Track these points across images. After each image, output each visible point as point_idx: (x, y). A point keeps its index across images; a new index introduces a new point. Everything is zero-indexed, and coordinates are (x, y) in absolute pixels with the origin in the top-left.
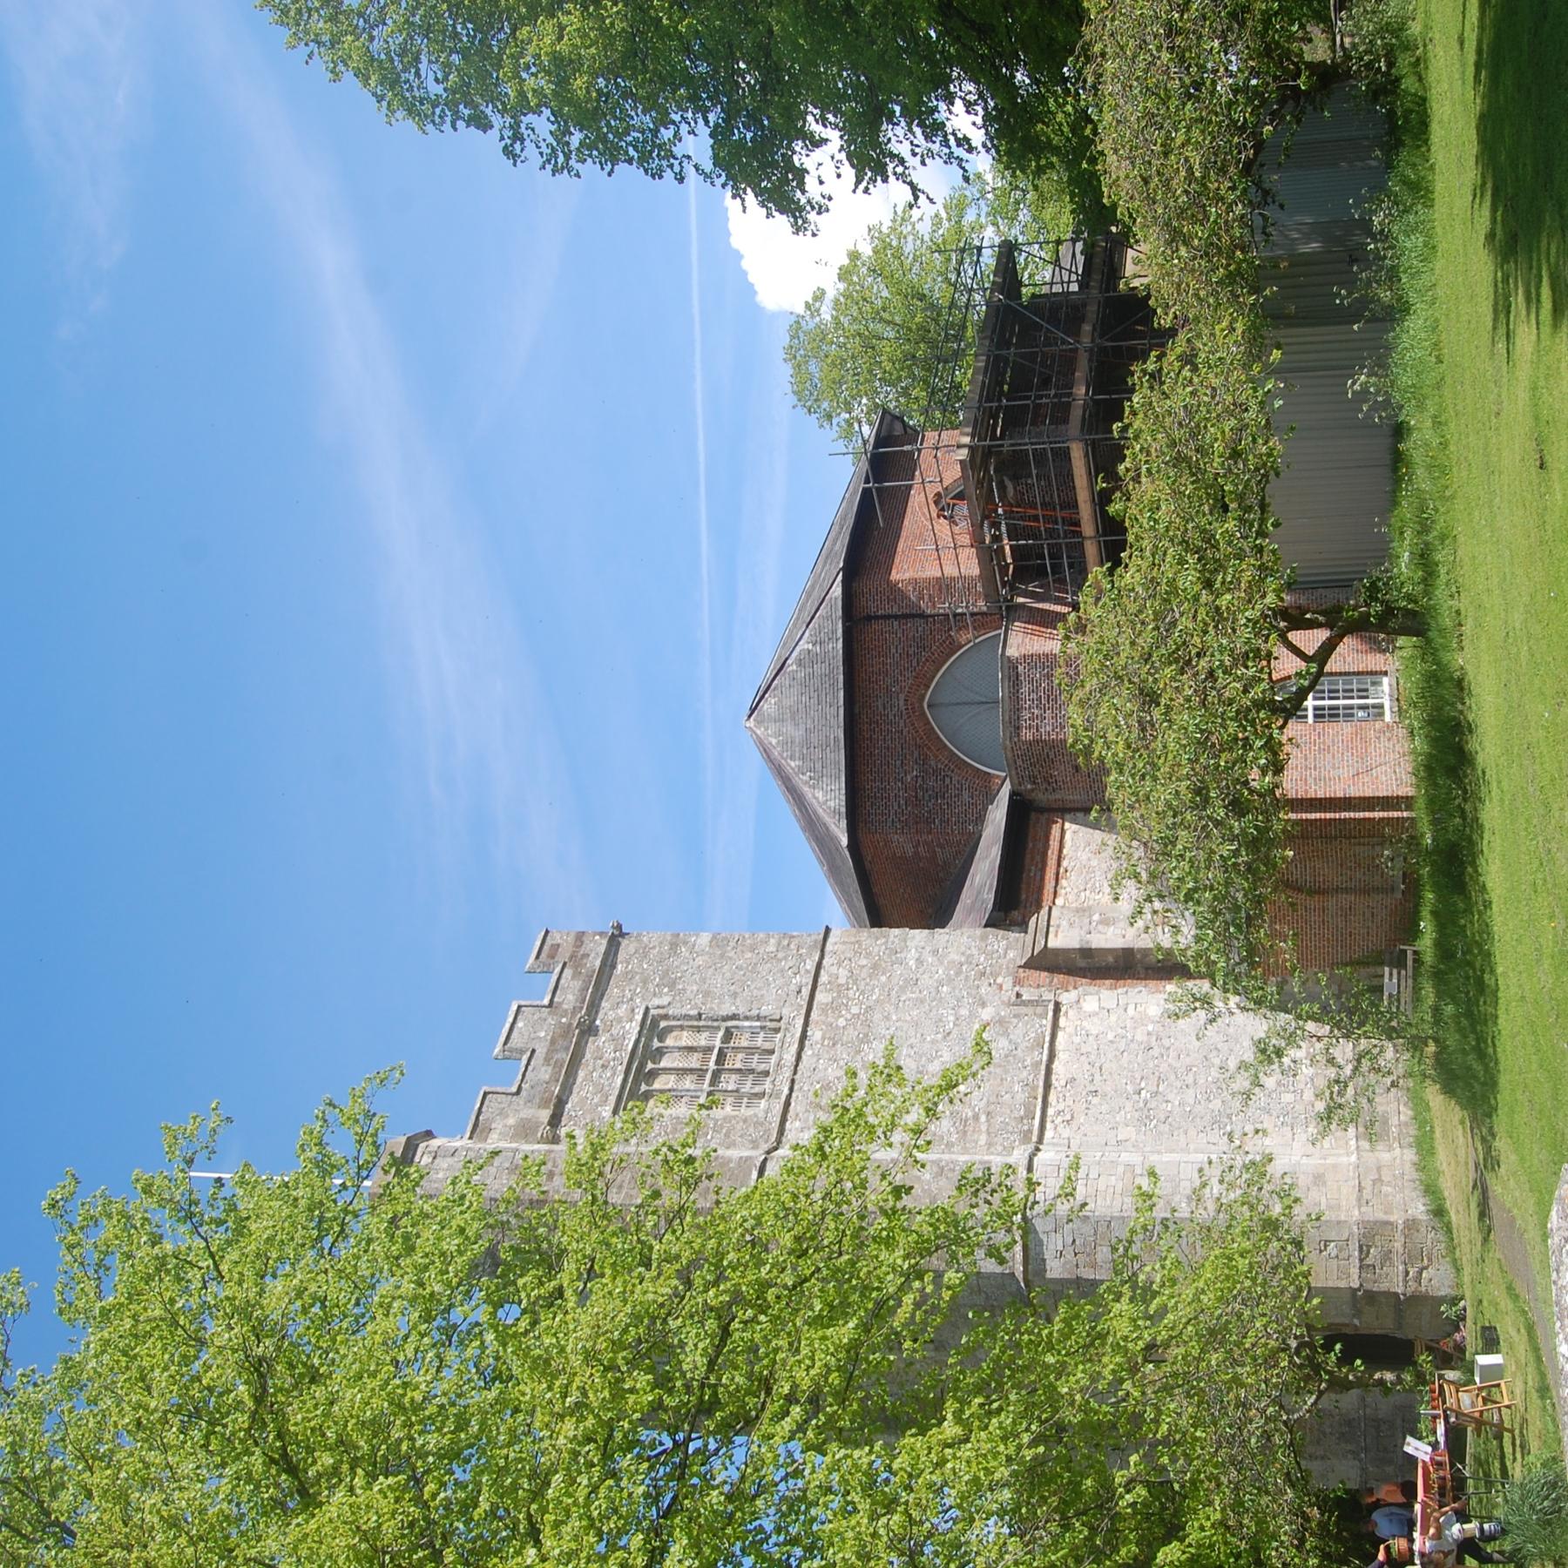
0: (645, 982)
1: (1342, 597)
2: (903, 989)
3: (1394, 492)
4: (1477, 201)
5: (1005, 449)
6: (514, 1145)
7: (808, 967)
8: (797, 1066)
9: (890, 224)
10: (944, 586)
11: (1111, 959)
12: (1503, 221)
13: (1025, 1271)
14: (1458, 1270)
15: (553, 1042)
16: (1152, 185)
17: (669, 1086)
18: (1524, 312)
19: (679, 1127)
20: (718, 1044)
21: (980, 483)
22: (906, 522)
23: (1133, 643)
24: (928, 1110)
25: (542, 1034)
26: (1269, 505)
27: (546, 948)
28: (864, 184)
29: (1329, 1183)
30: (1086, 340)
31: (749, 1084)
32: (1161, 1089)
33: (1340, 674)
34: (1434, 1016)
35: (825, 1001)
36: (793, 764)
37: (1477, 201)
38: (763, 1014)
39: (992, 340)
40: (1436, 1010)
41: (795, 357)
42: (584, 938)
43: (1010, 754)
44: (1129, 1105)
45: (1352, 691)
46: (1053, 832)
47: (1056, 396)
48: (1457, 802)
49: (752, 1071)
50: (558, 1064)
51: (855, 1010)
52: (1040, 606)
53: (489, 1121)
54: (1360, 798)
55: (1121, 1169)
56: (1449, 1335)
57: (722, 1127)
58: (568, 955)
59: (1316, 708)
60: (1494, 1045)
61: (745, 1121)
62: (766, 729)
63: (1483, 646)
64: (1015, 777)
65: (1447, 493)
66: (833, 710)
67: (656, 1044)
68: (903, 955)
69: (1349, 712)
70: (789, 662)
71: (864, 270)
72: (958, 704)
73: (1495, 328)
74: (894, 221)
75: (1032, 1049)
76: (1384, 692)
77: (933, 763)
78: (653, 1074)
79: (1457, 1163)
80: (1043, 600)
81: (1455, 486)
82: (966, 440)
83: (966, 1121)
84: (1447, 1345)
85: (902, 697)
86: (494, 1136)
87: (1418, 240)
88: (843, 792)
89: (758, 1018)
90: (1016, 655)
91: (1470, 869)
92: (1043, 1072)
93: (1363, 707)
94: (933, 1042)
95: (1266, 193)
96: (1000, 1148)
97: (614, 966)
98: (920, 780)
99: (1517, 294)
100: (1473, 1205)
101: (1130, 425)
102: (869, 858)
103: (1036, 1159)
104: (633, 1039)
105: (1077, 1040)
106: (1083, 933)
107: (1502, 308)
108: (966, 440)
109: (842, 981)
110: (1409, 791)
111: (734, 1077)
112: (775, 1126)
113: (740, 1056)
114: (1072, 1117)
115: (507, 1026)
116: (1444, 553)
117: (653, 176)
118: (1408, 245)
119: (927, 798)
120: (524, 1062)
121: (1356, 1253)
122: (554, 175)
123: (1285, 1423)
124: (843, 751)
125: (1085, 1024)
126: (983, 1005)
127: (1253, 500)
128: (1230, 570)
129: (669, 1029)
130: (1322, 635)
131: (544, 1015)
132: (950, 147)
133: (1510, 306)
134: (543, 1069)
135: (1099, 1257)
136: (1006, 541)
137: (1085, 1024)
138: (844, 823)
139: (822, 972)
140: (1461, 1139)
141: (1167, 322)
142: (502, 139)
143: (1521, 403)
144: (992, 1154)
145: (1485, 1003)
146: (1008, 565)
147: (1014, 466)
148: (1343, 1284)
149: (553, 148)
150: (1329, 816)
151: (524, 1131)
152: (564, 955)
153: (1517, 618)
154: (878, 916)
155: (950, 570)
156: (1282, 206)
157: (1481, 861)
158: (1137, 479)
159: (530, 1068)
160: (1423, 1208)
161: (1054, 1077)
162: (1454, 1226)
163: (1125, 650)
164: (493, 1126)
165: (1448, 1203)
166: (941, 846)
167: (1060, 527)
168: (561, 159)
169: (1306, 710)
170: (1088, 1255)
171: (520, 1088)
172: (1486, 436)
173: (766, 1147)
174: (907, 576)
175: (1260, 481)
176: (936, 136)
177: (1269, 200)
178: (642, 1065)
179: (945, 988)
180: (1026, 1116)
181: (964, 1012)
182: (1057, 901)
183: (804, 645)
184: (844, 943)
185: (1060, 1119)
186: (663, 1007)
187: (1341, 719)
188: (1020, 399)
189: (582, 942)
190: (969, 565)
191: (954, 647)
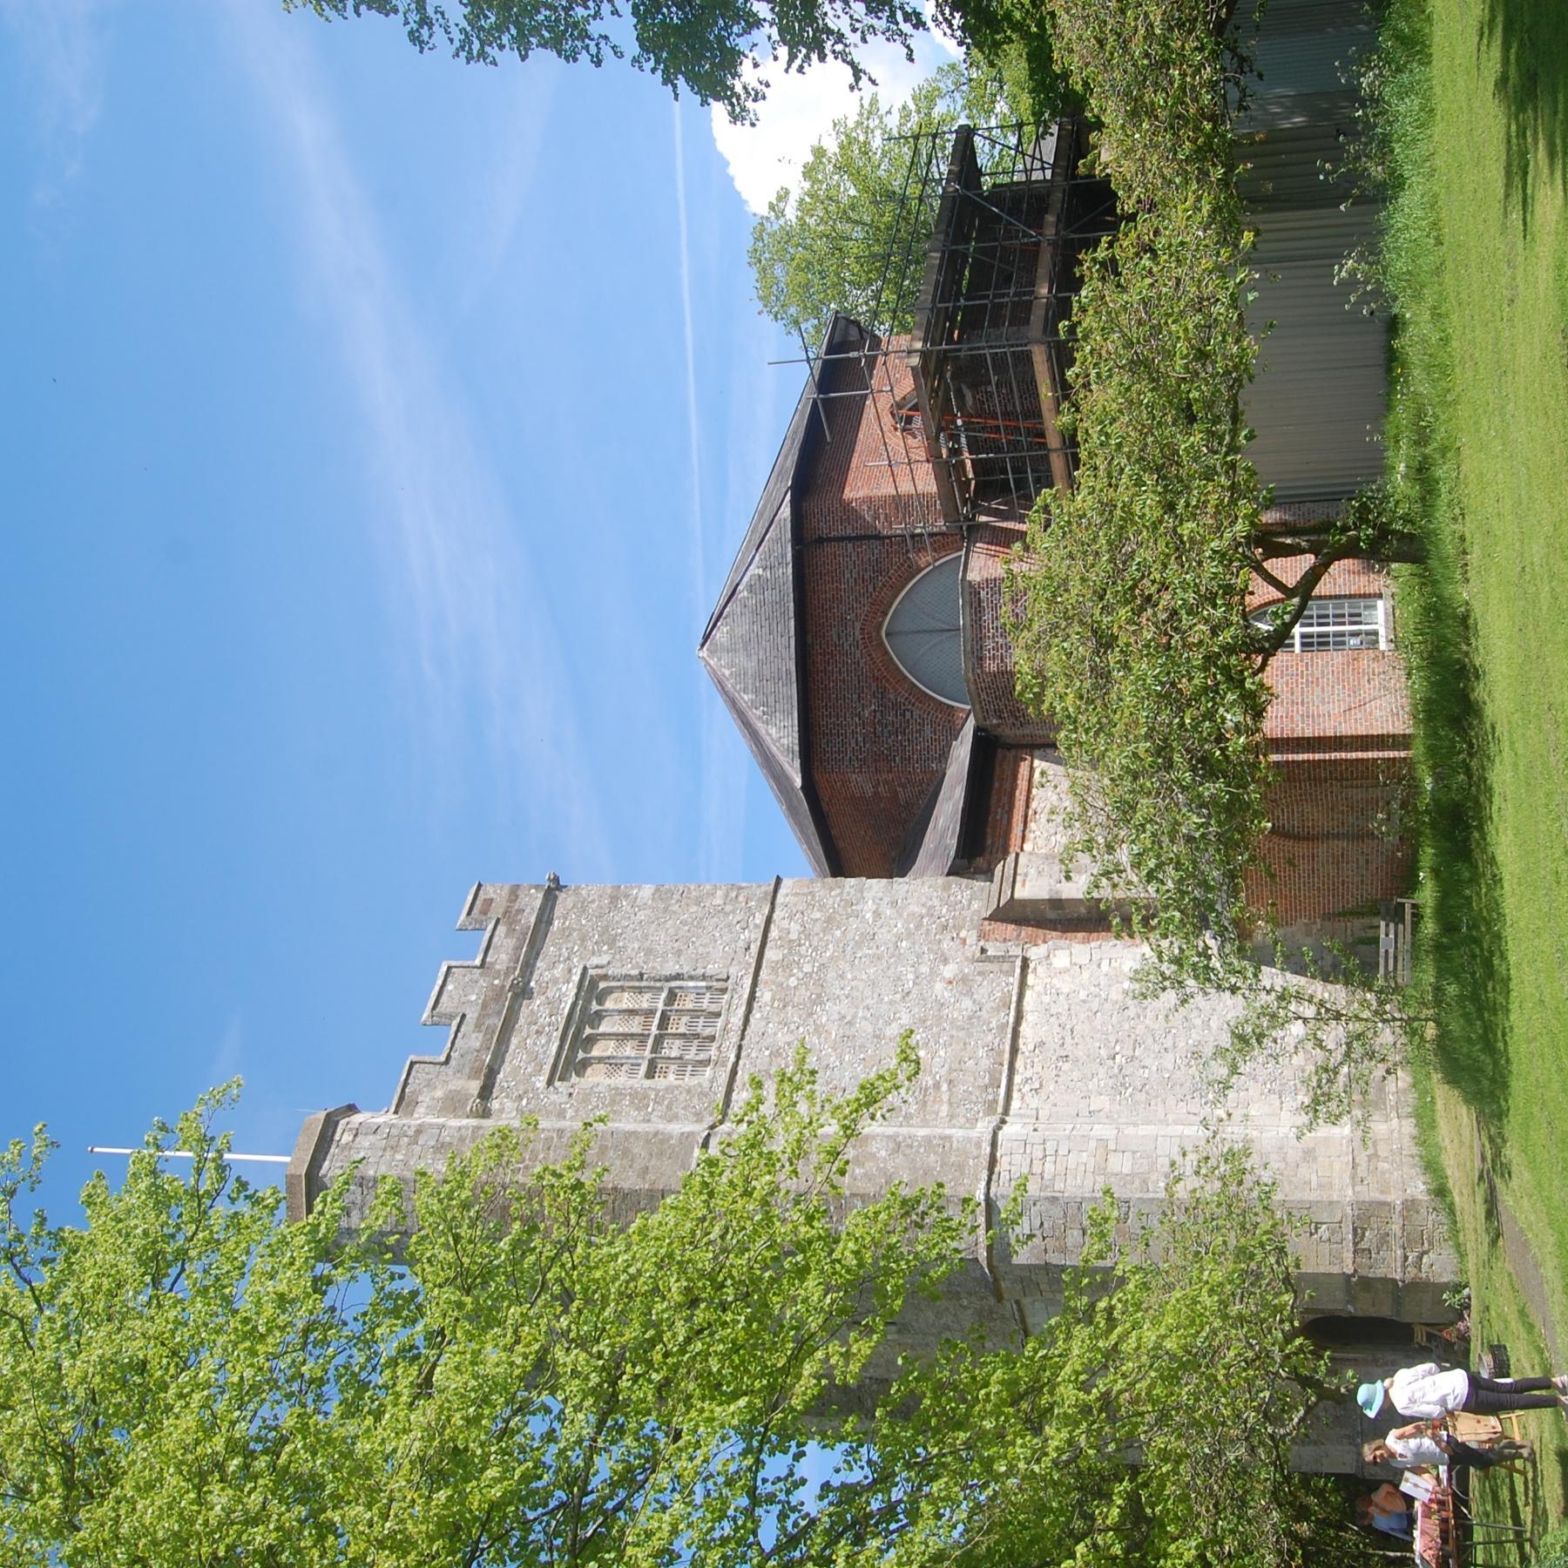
0: (583, 939)
1: (1332, 513)
2: (859, 945)
3: (1388, 395)
4: (1485, 41)
5: (962, 354)
6: (441, 1120)
7: (758, 922)
8: (744, 1031)
9: (857, 118)
10: (900, 504)
11: (1083, 910)
12: (1517, 60)
13: (989, 1258)
14: (1462, 1255)
15: (484, 1006)
16: (1108, 47)
17: (608, 1053)
18: (1546, 171)
19: (618, 1098)
20: (660, 1006)
21: (934, 391)
22: (860, 436)
23: (1083, 580)
24: (846, 1127)
25: (473, 998)
26: (1242, 413)
27: (479, 903)
28: (798, 62)
29: (1320, 1159)
30: (1050, 232)
31: (694, 1050)
32: (1137, 1053)
33: (1330, 597)
34: (1435, 996)
35: (775, 958)
36: (746, 697)
37: (1485, 41)
38: (709, 973)
39: (947, 234)
40: (1438, 990)
41: (760, 261)
42: (519, 892)
43: (973, 687)
44: (1102, 1071)
45: (1344, 616)
46: (1021, 770)
47: (1015, 294)
48: (1461, 756)
49: (697, 1036)
50: (489, 1031)
51: (807, 968)
52: (1004, 525)
53: (416, 1093)
54: (1352, 737)
55: (1093, 1144)
56: (1452, 1324)
57: (664, 1098)
58: (501, 910)
59: (1303, 636)
60: (1506, 1043)
61: (688, 1091)
62: (719, 659)
63: (1493, 580)
64: (979, 711)
65: (1449, 398)
66: (784, 641)
67: (595, 1007)
68: (859, 907)
69: (1339, 641)
70: (741, 588)
71: (830, 167)
72: (919, 632)
73: (1507, 196)
74: (861, 114)
75: (998, 1010)
76: (1379, 618)
77: (892, 696)
78: (591, 1041)
79: (1461, 1142)
80: (1006, 519)
81: (1458, 389)
82: (919, 345)
83: (926, 1090)
84: (1450, 1334)
85: (858, 625)
86: (421, 1110)
87: (1413, 103)
88: (796, 729)
89: (704, 977)
90: (978, 579)
91: (1476, 834)
92: (1009, 1036)
93: (1354, 634)
94: (891, 1003)
95: (1242, 60)
96: (962, 1120)
97: (550, 922)
98: (878, 715)
99: (1536, 149)
100: (1480, 1199)
101: (1079, 323)
102: (827, 799)
103: (1000, 1133)
104: (570, 1002)
105: (1047, 999)
106: (1052, 882)
107: (1517, 169)
108: (919, 345)
109: (794, 936)
110: (1400, 725)
111: (678, 1043)
112: (720, 1097)
113: (685, 1019)
114: (1041, 1085)
115: (437, 988)
116: (1445, 468)
117: (567, 59)
118: (1402, 109)
119: (886, 734)
120: (454, 1028)
121: (1350, 1236)
122: (468, 63)
123: (1272, 1437)
124: (795, 685)
125: (1055, 981)
126: (945, 961)
127: (1222, 408)
128: (1195, 492)
129: (609, 991)
130: (1308, 560)
131: (475, 977)
132: (897, 24)
133: (1527, 165)
134: (474, 1035)
135: (1070, 1242)
136: (966, 454)
137: (1055, 981)
138: (797, 763)
139: (772, 926)
140: (1465, 1119)
141: (1129, 206)
142: (406, 23)
143: (1542, 288)
144: (954, 1127)
145: (1494, 989)
146: (969, 481)
147: (971, 372)
148: (1335, 1270)
149: (466, 33)
150: (1318, 756)
151: (452, 1104)
152: (497, 911)
153: (1537, 551)
154: (838, 864)
155: (906, 488)
156: (1260, 76)
157: (1490, 828)
158: (1086, 386)
159: (460, 1035)
160: (1423, 1187)
161: (1021, 1041)
162: (1458, 1209)
163: (1075, 587)
164: (420, 1099)
165: (1451, 1182)
166: (903, 786)
167: (1023, 439)
168: (476, 46)
169: (1293, 638)
170: (1058, 1239)
171: (448, 1057)
172: (1496, 328)
173: (709, 1120)
174: (861, 494)
175: (1231, 387)
176: (881, 11)
177: (1246, 69)
178: (579, 1030)
179: (904, 944)
180: (991, 1085)
181: (924, 969)
182: (1025, 846)
183: (754, 570)
184: (796, 894)
185: (1027, 1087)
186: (602, 967)
187: (1331, 647)
188: (981, 298)
189: (517, 897)
190: (926, 482)
191: (914, 570)
